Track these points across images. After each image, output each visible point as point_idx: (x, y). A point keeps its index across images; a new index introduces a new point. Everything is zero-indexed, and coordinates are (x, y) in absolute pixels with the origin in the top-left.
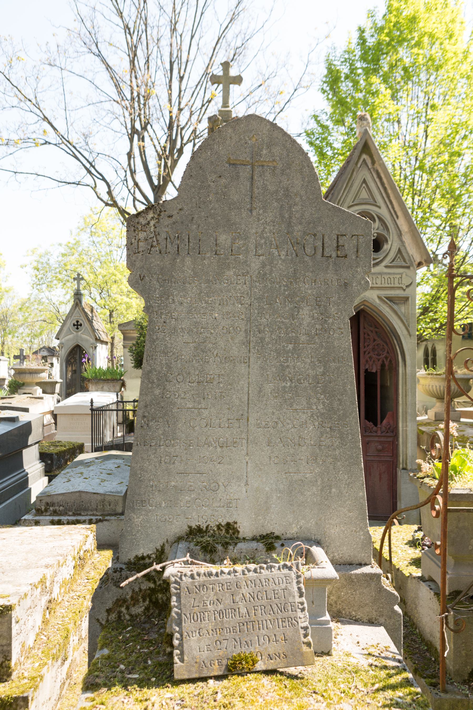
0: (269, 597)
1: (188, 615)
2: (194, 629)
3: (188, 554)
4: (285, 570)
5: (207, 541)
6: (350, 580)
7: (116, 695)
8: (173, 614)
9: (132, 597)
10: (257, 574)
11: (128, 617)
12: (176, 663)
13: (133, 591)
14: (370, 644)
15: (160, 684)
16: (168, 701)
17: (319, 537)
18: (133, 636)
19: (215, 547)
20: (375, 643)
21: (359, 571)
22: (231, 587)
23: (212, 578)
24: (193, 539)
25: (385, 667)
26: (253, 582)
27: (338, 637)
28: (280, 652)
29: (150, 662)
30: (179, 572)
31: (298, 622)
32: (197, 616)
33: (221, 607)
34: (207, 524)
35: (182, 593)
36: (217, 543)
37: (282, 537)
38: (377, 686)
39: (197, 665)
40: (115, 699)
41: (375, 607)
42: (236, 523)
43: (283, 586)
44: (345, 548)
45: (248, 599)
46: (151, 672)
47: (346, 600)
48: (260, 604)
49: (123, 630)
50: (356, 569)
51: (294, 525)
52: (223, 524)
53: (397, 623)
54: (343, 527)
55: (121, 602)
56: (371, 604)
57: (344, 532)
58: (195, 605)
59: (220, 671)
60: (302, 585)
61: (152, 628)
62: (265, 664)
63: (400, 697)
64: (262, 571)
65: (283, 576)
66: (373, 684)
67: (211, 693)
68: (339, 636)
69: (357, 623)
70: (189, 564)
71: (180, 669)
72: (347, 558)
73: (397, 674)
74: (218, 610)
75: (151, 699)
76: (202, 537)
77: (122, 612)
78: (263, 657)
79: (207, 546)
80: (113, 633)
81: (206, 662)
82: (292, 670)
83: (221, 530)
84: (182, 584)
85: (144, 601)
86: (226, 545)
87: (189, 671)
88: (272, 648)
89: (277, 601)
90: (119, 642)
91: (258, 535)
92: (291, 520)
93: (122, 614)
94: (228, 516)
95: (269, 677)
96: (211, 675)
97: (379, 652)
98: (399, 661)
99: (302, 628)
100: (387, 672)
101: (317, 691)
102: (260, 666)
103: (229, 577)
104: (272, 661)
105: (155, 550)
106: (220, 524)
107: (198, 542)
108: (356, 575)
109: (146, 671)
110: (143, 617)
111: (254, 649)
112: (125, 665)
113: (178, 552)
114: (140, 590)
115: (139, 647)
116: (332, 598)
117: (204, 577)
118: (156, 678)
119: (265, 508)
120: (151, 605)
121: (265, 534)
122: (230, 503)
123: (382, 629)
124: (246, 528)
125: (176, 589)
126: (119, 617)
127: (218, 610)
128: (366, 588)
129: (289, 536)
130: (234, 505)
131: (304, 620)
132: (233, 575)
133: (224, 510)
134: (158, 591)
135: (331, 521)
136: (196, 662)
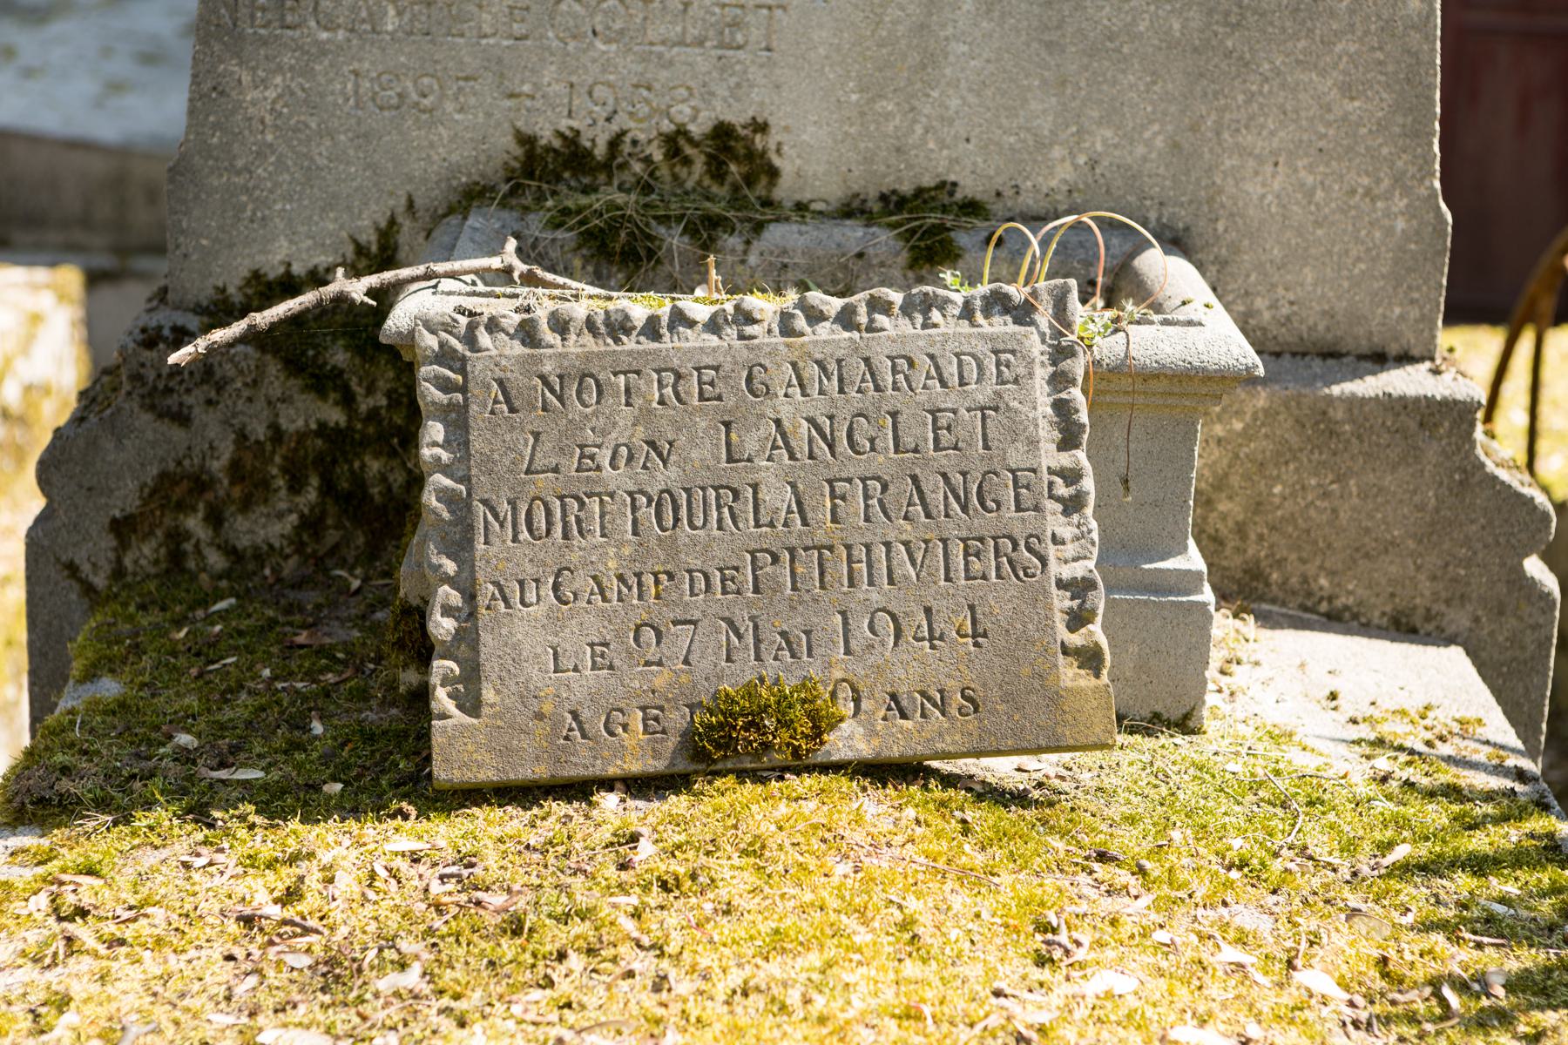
0: (908, 441)
1: (504, 508)
2: (530, 569)
3: (512, 244)
4: (997, 319)
5: (612, 206)
6: (1323, 426)
7: (158, 841)
8: (430, 499)
9: (235, 467)
10: (856, 335)
11: (216, 560)
12: (444, 716)
13: (242, 436)
14: (1388, 704)
15: (366, 799)
16: (402, 865)
17: (1181, 216)
18: (241, 633)
19: (649, 237)
20: (1414, 705)
21: (1370, 386)
22: (721, 387)
23: (629, 343)
24: (540, 198)
25: (1453, 792)
26: (832, 367)
27: (1234, 667)
28: (952, 685)
29: (318, 728)
30: (461, 311)
31: (1044, 561)
32: (549, 513)
33: (665, 476)
34: (615, 127)
35: (474, 408)
36: (664, 220)
37: (997, 207)
38: (1401, 852)
39: (541, 728)
40: (150, 858)
41: (1432, 560)
42: (762, 127)
43: (983, 393)
44: (1309, 275)
45: (801, 448)
46: (325, 759)
47: (1292, 519)
48: (861, 471)
49: (192, 608)
50: (1357, 375)
51: (1057, 152)
52: (695, 130)
53: (1529, 637)
54: (1310, 169)
55: (178, 488)
56: (1411, 544)
57: (1310, 194)
58: (537, 465)
59: (656, 755)
60: (1076, 394)
61: (333, 605)
62: (872, 733)
63: (1503, 900)
64: (881, 320)
65: (982, 348)
66: (1386, 847)
67: (608, 837)
68: (1245, 668)
69: (1335, 624)
70: (511, 282)
71: (459, 742)
72: (1313, 324)
73: (1504, 819)
74: (654, 491)
75: (319, 854)
76: (586, 191)
77: (187, 535)
78: (865, 705)
79: (613, 228)
80: (144, 621)
81: (585, 714)
82: (1001, 769)
83: (687, 162)
84: (478, 367)
85: (296, 487)
86: (706, 231)
87: (506, 752)
88: (909, 667)
89: (946, 460)
90: (174, 654)
91: (873, 193)
92: (1045, 125)
93: (188, 546)
94: (722, 91)
95: (890, 790)
96: (612, 771)
97: (1429, 736)
98: (1520, 775)
99: (1061, 584)
100: (1456, 808)
101: (1113, 852)
102: (849, 740)
103: (713, 340)
104: (908, 724)
105: (349, 250)
106: (682, 132)
107: (566, 212)
108: (1353, 402)
109: (300, 756)
110: (293, 562)
111: (828, 667)
112: (199, 736)
113: (464, 238)
114: (277, 434)
115: (267, 672)
116: (1223, 506)
117: (588, 338)
118: (346, 783)
119: (914, 58)
120: (332, 509)
121: (906, 188)
122: (735, 24)
123: (1456, 656)
124: (813, 151)
125: (445, 386)
126: (176, 558)
127: (654, 491)
128: (1394, 468)
129: (1028, 201)
130: (756, 34)
131: (1073, 548)
132: (731, 332)
133: (702, 61)
134: (364, 443)
135: (1247, 139)
136: (539, 716)
